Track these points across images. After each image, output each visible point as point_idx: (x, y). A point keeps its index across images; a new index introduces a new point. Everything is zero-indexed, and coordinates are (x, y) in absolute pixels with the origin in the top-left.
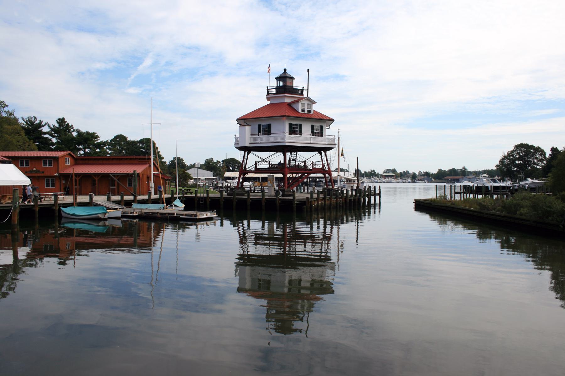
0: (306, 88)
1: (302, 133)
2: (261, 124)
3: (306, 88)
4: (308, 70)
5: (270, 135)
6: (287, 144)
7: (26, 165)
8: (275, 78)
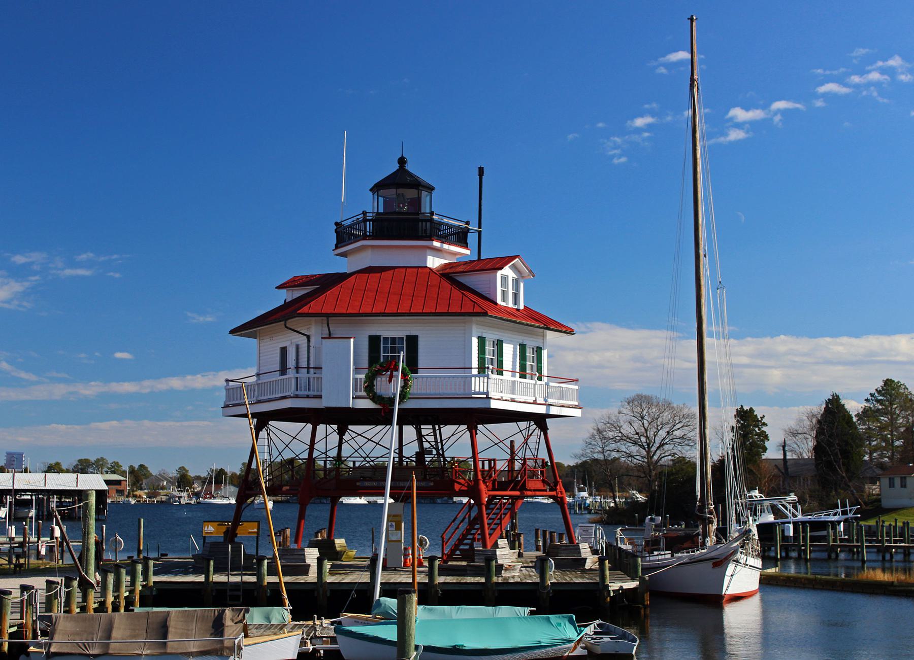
0: (473, 227)
2: (378, 334)
4: (481, 171)
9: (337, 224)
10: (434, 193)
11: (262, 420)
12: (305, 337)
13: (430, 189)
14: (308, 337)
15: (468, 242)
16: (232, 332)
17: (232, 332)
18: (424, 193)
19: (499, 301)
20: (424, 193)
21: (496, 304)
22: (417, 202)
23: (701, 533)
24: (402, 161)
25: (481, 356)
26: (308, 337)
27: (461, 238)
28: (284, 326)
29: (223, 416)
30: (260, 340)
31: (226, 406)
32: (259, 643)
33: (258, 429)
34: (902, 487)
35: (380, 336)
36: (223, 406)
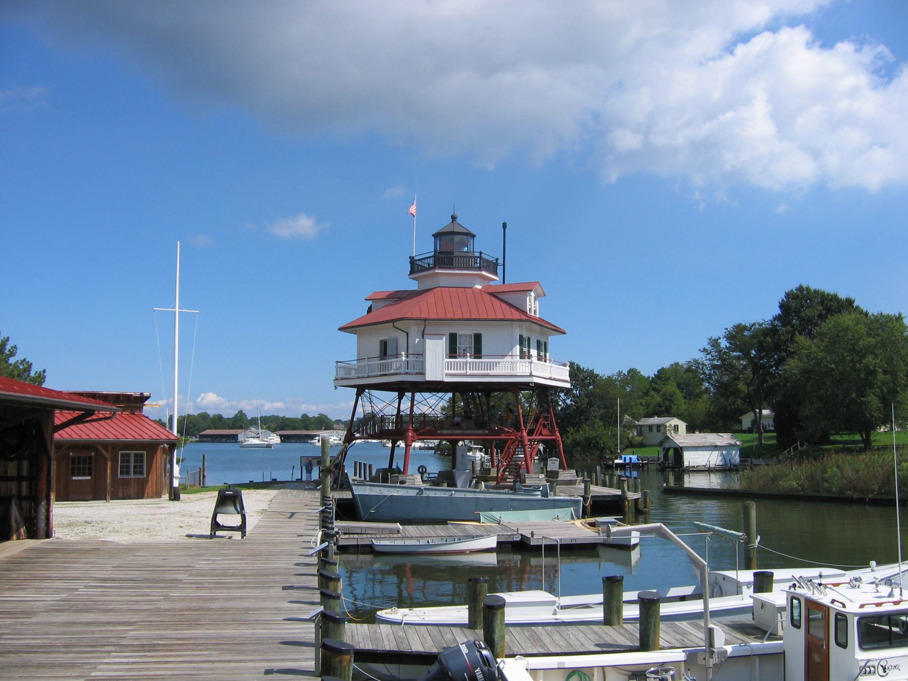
0: (501, 261)
1: (483, 353)
2: (456, 332)
3: (501, 261)
4: (505, 226)
5: (480, 358)
6: (536, 380)
7: (135, 473)
8: (433, 236)
11: (361, 390)
12: (405, 334)
14: (407, 334)
17: (341, 329)
19: (528, 312)
21: (527, 313)
26: (407, 334)
27: (492, 267)
28: (392, 326)
31: (337, 379)
32: (302, 536)
33: (358, 394)
34: (658, 431)
35: (457, 334)
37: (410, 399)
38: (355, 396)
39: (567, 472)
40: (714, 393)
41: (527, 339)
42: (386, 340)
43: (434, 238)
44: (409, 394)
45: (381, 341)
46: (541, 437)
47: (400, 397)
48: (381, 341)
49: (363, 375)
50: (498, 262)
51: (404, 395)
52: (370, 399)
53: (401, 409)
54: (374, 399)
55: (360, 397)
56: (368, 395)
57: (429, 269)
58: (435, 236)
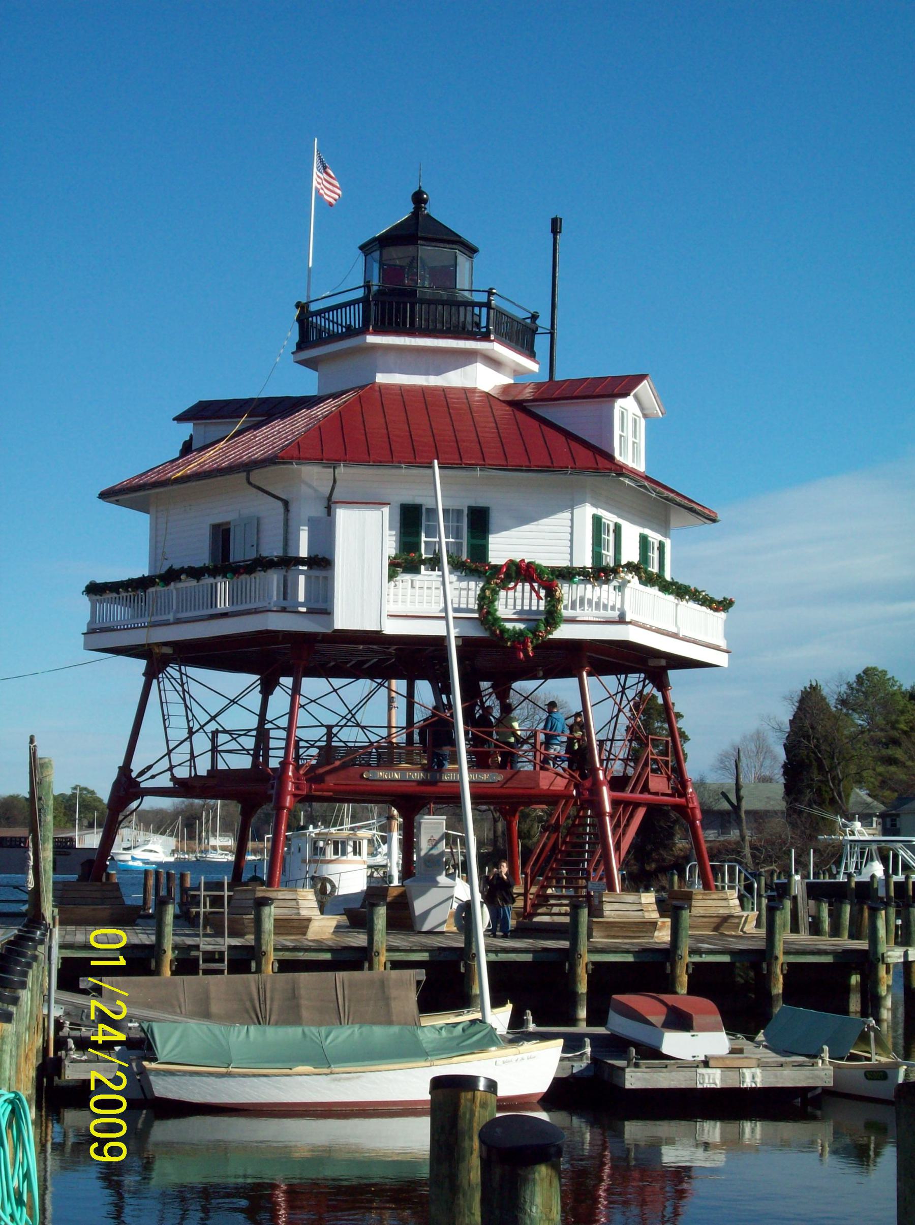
0: (544, 322)
2: (418, 501)
4: (556, 226)
9: (298, 305)
10: (477, 258)
13: (471, 250)
14: (286, 503)
15: (535, 349)
16: (104, 495)
17: (104, 495)
18: (462, 260)
20: (462, 260)
22: (451, 273)
23: (846, 838)
24: (419, 199)
25: (597, 549)
26: (286, 503)
28: (245, 481)
29: (85, 649)
30: (157, 512)
33: (151, 674)
36: (85, 631)
37: (290, 692)
38: (143, 679)
39: (714, 896)
40: (865, 903)
41: (612, 528)
42: (228, 523)
43: (366, 256)
44: (287, 681)
45: (216, 528)
46: (646, 796)
47: (267, 689)
48: (216, 528)
49: (165, 617)
50: (538, 322)
51: (278, 683)
52: (182, 685)
53: (269, 717)
54: (194, 688)
55: (155, 682)
56: (177, 675)
57: (350, 332)
58: (365, 248)
